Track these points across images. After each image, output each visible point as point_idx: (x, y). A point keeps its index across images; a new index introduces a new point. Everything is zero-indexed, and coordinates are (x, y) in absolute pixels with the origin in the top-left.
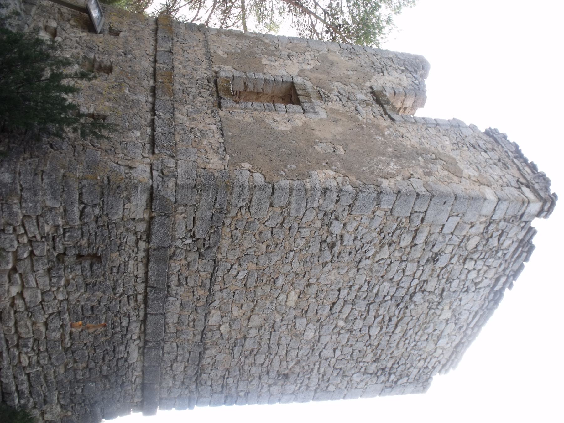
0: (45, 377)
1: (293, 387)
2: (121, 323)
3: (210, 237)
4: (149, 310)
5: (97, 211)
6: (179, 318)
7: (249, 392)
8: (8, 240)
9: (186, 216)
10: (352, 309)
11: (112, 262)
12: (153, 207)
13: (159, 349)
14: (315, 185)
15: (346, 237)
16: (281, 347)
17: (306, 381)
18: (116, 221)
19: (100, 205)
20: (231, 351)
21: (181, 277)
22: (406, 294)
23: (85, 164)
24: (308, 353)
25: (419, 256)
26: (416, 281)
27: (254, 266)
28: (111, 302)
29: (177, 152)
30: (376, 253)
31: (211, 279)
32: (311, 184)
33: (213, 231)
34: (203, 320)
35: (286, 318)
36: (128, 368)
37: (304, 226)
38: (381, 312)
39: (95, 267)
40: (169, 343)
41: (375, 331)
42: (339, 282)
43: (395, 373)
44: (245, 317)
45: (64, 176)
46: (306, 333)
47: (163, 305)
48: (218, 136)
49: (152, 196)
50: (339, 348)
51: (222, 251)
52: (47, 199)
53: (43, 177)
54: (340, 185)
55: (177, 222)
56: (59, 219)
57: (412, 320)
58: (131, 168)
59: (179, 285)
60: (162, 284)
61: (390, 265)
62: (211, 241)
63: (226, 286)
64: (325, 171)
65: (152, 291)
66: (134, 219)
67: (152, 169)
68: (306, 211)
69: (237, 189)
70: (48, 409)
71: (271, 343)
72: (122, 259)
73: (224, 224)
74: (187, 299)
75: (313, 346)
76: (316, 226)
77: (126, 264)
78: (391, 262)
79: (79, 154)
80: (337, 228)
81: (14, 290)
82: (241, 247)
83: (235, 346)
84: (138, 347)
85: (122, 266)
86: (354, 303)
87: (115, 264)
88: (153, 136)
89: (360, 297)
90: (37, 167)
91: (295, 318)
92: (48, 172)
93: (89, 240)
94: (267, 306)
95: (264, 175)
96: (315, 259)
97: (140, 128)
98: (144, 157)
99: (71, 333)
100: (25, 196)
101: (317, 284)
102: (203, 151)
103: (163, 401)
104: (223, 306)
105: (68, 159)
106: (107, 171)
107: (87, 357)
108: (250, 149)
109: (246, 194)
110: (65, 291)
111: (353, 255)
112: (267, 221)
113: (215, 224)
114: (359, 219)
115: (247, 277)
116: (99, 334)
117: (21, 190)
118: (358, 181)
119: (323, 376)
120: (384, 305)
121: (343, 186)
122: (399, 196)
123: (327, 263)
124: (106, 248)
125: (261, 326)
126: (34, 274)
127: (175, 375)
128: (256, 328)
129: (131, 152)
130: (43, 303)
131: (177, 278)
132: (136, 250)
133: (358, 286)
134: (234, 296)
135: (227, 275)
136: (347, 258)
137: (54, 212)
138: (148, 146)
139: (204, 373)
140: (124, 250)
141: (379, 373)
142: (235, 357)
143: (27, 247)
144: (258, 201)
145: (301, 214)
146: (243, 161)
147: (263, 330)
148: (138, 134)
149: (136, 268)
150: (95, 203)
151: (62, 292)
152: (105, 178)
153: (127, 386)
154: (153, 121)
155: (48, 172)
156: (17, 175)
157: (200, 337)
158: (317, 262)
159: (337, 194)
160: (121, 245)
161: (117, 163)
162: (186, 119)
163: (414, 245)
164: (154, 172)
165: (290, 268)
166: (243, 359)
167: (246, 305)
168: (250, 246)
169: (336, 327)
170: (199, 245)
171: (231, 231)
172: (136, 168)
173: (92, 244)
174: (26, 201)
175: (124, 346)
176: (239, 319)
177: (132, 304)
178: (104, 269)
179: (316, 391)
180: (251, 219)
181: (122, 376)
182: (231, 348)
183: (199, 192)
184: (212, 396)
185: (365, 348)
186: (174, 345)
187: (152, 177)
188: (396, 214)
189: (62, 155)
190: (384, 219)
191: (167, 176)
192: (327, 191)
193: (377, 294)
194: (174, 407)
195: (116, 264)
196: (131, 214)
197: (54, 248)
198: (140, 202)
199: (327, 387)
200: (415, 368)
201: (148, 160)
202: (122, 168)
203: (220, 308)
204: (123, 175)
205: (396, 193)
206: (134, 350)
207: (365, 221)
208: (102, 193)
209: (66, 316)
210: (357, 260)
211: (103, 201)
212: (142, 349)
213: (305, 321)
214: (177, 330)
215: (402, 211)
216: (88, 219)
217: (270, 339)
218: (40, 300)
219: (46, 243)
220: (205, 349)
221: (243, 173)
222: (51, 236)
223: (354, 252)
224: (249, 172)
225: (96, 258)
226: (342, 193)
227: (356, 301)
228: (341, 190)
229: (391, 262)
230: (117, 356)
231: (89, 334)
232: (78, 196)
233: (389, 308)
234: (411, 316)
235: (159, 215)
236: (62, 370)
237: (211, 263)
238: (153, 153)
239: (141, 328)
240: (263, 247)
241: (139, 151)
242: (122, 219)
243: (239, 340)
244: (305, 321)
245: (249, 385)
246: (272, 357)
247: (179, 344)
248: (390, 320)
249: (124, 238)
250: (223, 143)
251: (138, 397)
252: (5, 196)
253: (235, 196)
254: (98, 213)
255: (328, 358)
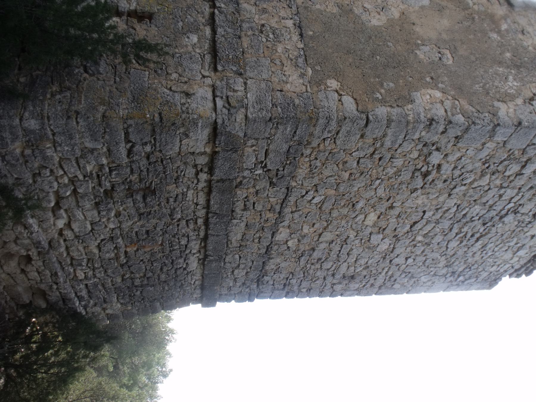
0: (103, 285)
1: (357, 286)
2: (179, 242)
3: (284, 167)
4: (210, 232)
5: (148, 148)
6: (243, 236)
7: (311, 289)
8: (46, 182)
9: (257, 149)
10: (434, 227)
11: (168, 193)
12: (217, 142)
13: (220, 261)
14: (419, 114)
15: (445, 166)
16: (351, 256)
17: (372, 281)
18: (172, 156)
19: (151, 142)
20: (297, 260)
21: (247, 203)
22: (497, 215)
23: (129, 94)
24: (379, 261)
25: (523, 183)
26: (512, 205)
27: (333, 192)
28: (168, 227)
29: (245, 65)
30: (475, 180)
31: (282, 204)
32: (413, 114)
33: (288, 162)
34: (270, 237)
35: (361, 234)
36: (187, 274)
37: (397, 156)
38: (465, 229)
39: (149, 199)
40: (231, 255)
41: (453, 244)
42: (426, 206)
43: (464, 275)
44: (315, 234)
45: (104, 116)
46: (380, 246)
47: (226, 228)
48: (296, 38)
49: (215, 132)
50: (413, 257)
51: (297, 179)
52: (86, 141)
53: (78, 120)
54: (449, 114)
55: (246, 154)
56: (103, 159)
57: (496, 235)
58: (188, 95)
59: (245, 209)
60: (226, 211)
61: (487, 191)
62: (285, 172)
63: (298, 209)
64: (430, 91)
65: (214, 216)
66: (194, 153)
67: (214, 96)
68: (403, 142)
69: (321, 121)
70: (109, 306)
71: (341, 253)
72: (180, 190)
73: (302, 154)
74: (254, 221)
75: (386, 255)
76: (411, 156)
77: (184, 194)
78: (489, 189)
79: (121, 78)
80: (436, 158)
81: (61, 223)
82: (321, 176)
83: (302, 256)
84: (197, 259)
85: (180, 197)
86: (437, 222)
87: (172, 195)
88: (214, 42)
89: (446, 218)
90: (70, 106)
91: (370, 234)
92: (83, 113)
93: (140, 175)
94: (342, 225)
95: (355, 99)
96: (404, 186)
97: (196, 30)
98: (204, 77)
99: (126, 252)
100: (59, 141)
101: (401, 206)
102: (278, 62)
103: (223, 296)
104: (292, 225)
105: (108, 88)
106: (158, 104)
107: (144, 270)
108: (337, 57)
109: (333, 125)
110: (116, 220)
111: (448, 183)
112: (355, 151)
113: (291, 157)
114: (464, 151)
115: (323, 202)
116: (156, 252)
117: (54, 135)
118: (471, 108)
119: (390, 277)
120: (470, 224)
121: (453, 115)
122: (519, 128)
123: (416, 190)
124: (161, 182)
125: (333, 241)
126: (80, 209)
127: (236, 278)
128: (327, 242)
129: (187, 70)
130: (93, 231)
131: (243, 204)
132: (196, 181)
133: (446, 208)
134: (306, 217)
135: (301, 199)
136: (440, 185)
137: (96, 153)
138: (208, 58)
139: (267, 276)
140: (182, 182)
141: (449, 275)
142: (301, 264)
143: (69, 187)
144: (347, 132)
145: (397, 146)
146: (329, 77)
147: (334, 244)
148: (194, 39)
149: (196, 196)
150: (144, 141)
151: (114, 222)
152: (157, 115)
153: (187, 287)
154: (213, 15)
155: (83, 113)
156: (46, 121)
157: (265, 250)
158: (405, 189)
159: (444, 127)
160: (178, 178)
161: (170, 89)
162: (254, 11)
163: (519, 174)
164: (218, 100)
165: (373, 193)
166: (308, 266)
167: (318, 224)
168: (330, 174)
169: (413, 240)
170: (270, 176)
171: (310, 161)
172: (194, 94)
173: (144, 180)
174: (60, 145)
175: (183, 259)
176: (309, 235)
177: (192, 226)
178: (158, 200)
179: (380, 287)
180: (335, 150)
181: (181, 280)
182: (298, 257)
183: (275, 125)
184: (273, 292)
185: (439, 257)
186: (237, 256)
187: (215, 109)
188: (509, 146)
189: (101, 83)
190: (494, 150)
191: (235, 108)
192: (434, 123)
193: (465, 215)
194: (234, 299)
195: (173, 195)
196: (189, 149)
197: (100, 185)
198: (200, 137)
199: (393, 285)
200: (486, 271)
201: (208, 81)
202: (177, 96)
203: (289, 227)
204: (179, 107)
205: (515, 126)
206: (194, 262)
207: (471, 153)
208: (154, 131)
209: (120, 240)
210: (452, 187)
211: (155, 139)
212: (202, 260)
213: (381, 236)
214: (241, 246)
215: (517, 144)
216: (137, 157)
217: (340, 251)
218: (90, 229)
219: (90, 182)
220: (269, 258)
221: (330, 97)
222: (95, 175)
223: (449, 180)
224: (336, 94)
225: (149, 192)
226: (451, 126)
227: (440, 220)
228: (450, 122)
229: (489, 189)
230: (175, 267)
231: (145, 253)
232: (123, 135)
233: (475, 226)
234: (496, 232)
235: (223, 150)
236: (119, 280)
237: (284, 190)
238: (215, 70)
239: (201, 244)
240: (346, 175)
241: (197, 67)
242: (179, 153)
243: (307, 252)
244: (381, 236)
245: (312, 284)
246: (340, 263)
247: (242, 256)
248: (472, 236)
249: (182, 171)
250: (303, 49)
251: (197, 294)
252: (34, 142)
253: (318, 129)
254: (149, 150)
255: (399, 265)
